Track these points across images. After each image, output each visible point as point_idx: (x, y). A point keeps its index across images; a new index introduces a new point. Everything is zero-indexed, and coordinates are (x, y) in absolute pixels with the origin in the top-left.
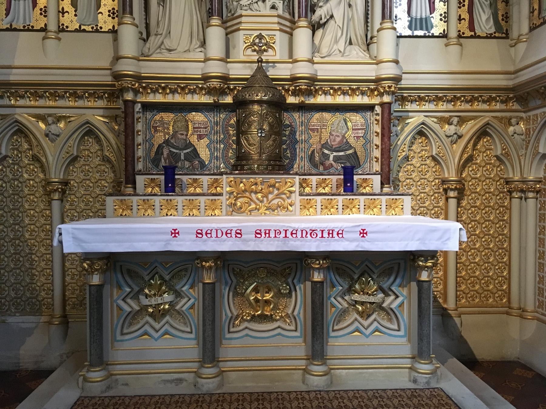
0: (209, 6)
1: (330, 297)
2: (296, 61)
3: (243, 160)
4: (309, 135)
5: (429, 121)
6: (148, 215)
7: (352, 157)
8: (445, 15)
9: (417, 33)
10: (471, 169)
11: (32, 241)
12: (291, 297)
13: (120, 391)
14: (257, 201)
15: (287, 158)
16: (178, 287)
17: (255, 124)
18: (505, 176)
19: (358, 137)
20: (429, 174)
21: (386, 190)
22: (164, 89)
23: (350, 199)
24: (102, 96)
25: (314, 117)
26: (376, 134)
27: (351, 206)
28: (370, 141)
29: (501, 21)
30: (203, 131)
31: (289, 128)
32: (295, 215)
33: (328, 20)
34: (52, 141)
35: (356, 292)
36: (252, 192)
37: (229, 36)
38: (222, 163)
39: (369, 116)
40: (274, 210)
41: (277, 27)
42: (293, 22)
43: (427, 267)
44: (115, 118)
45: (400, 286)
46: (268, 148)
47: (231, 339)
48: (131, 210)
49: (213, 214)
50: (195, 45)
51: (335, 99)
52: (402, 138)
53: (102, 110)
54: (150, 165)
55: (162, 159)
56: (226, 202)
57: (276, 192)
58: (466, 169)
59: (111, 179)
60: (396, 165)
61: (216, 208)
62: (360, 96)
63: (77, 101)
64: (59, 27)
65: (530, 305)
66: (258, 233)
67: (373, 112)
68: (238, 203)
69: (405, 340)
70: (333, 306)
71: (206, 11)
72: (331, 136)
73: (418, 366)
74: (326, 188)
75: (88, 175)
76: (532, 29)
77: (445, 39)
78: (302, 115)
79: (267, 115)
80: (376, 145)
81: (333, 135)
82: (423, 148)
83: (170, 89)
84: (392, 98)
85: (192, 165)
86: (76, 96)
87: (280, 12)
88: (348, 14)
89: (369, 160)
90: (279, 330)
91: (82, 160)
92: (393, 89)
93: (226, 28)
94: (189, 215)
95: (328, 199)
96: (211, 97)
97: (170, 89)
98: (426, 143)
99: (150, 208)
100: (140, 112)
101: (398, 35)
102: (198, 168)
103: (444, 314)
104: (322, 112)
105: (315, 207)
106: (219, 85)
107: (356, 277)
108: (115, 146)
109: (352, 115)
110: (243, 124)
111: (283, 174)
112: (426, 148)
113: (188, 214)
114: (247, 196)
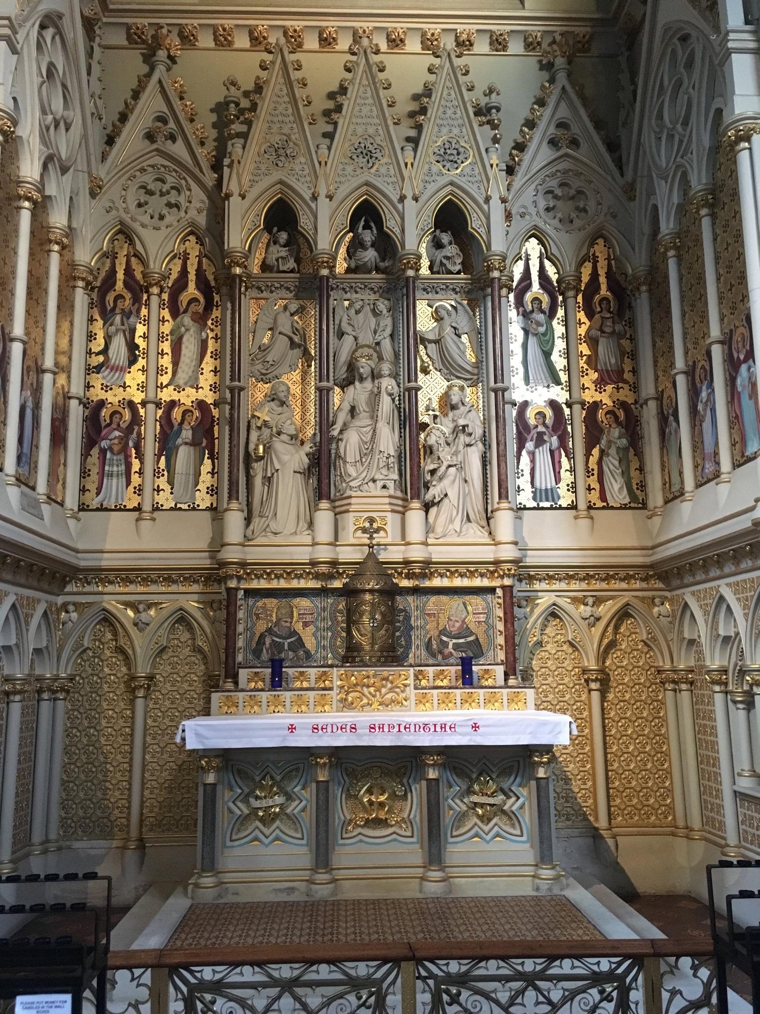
1: (448, 798)
2: (408, 544)
5: (560, 601)
9: (542, 504)
10: (615, 656)
11: (108, 747)
12: (406, 800)
13: (230, 899)
16: (289, 789)
18: (656, 664)
19: (479, 622)
20: (567, 662)
21: (512, 682)
22: (269, 574)
27: (470, 700)
29: (636, 491)
30: (309, 618)
32: (410, 710)
33: (442, 499)
34: (141, 630)
35: (475, 793)
36: (364, 686)
37: (338, 516)
40: (387, 706)
41: (388, 507)
43: (543, 763)
45: (520, 786)
47: (344, 845)
52: (532, 620)
53: (197, 595)
54: (250, 657)
57: (389, 685)
58: (610, 656)
60: (528, 652)
62: (480, 578)
65: (696, 823)
66: (372, 728)
69: (528, 845)
70: (451, 808)
73: (541, 872)
74: (445, 681)
76: (667, 502)
77: (574, 511)
86: (169, 580)
87: (391, 491)
88: (464, 491)
90: (394, 836)
92: (513, 572)
103: (595, 835)
107: (474, 776)
108: (210, 635)
111: (396, 666)
112: (561, 632)
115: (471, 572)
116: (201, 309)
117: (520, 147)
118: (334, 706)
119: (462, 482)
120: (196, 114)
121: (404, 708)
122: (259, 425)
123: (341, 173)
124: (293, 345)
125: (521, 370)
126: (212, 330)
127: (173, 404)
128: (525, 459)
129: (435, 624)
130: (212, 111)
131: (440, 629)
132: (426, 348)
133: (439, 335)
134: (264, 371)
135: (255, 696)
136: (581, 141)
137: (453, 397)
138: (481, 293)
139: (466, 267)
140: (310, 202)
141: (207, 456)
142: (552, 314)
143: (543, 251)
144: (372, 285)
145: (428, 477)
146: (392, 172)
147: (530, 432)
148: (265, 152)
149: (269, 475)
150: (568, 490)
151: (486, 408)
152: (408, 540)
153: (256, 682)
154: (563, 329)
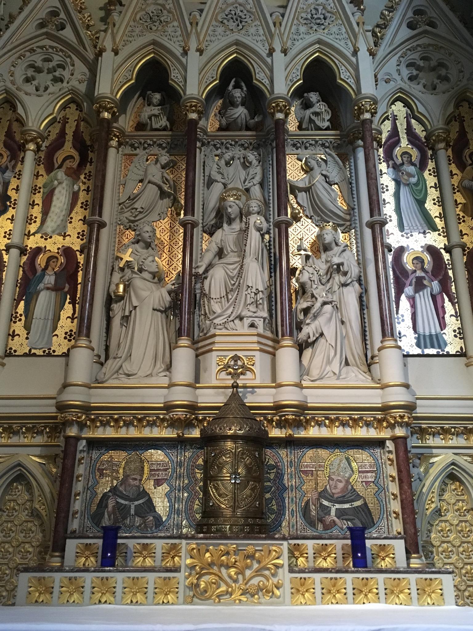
0: (178, 326)
2: (280, 386)
3: (211, 517)
4: (301, 479)
5: (460, 460)
6: (74, 602)
7: (361, 510)
8: (460, 331)
14: (229, 580)
15: (272, 512)
17: (228, 466)
19: (367, 483)
22: (117, 421)
23: (363, 579)
24: (42, 431)
25: (307, 455)
26: (391, 479)
27: (365, 590)
28: (384, 489)
30: (162, 475)
31: (275, 470)
32: (283, 603)
33: (317, 339)
36: (222, 565)
37: (200, 358)
38: (184, 520)
39: (379, 454)
40: (253, 596)
41: (257, 347)
42: (277, 341)
44: (52, 459)
46: (244, 500)
48: (51, 593)
49: (165, 601)
50: (160, 368)
51: (332, 431)
52: (428, 483)
53: (40, 448)
54: (88, 523)
55: (106, 513)
56: (185, 581)
57: (256, 566)
59: (38, 541)
60: (425, 522)
61: (170, 592)
62: (365, 428)
63: (11, 438)
64: (6, 351)
67: (383, 448)
68: (202, 583)
71: (176, 331)
72: (331, 482)
74: (329, 559)
75: (10, 536)
77: (464, 358)
78: (291, 453)
79: (243, 454)
80: (393, 494)
81: (333, 480)
82: (459, 498)
83: (124, 421)
84: (407, 431)
85: (145, 522)
87: (261, 330)
89: (385, 516)
91: (5, 514)
92: (406, 420)
93: (197, 349)
94: (132, 602)
95: (331, 579)
96: (174, 430)
97: (124, 421)
98: (462, 490)
99: (78, 591)
100: (84, 451)
101: (405, 354)
102: (152, 527)
104: (317, 448)
105: (312, 590)
106: (184, 416)
108: (48, 495)
109: (356, 452)
110: (212, 467)
111: (265, 539)
112: (462, 497)
113: (129, 601)
114: (214, 572)
115: (354, 420)
116: (75, 165)
117: (383, 26)
118: (181, 595)
119: (339, 323)
120: (85, 8)
121: (274, 599)
122: (121, 266)
123: (211, 33)
124: (163, 194)
125: (395, 217)
126: (84, 183)
127: (38, 250)
128: (404, 303)
129: (312, 484)
130: (101, 9)
131: (319, 490)
132: (296, 197)
133: (310, 183)
134: (133, 219)
135: (76, 578)
136: (438, 23)
137: (326, 236)
138: (350, 147)
139: (335, 124)
140: (181, 57)
141: (68, 300)
142: (422, 166)
143: (409, 112)
144: (243, 142)
145: (301, 317)
146: (261, 32)
147: (408, 277)
148: (140, 19)
149: (127, 313)
150: (456, 336)
151: (360, 253)
152: (279, 381)
153: (87, 558)
154: (435, 180)
